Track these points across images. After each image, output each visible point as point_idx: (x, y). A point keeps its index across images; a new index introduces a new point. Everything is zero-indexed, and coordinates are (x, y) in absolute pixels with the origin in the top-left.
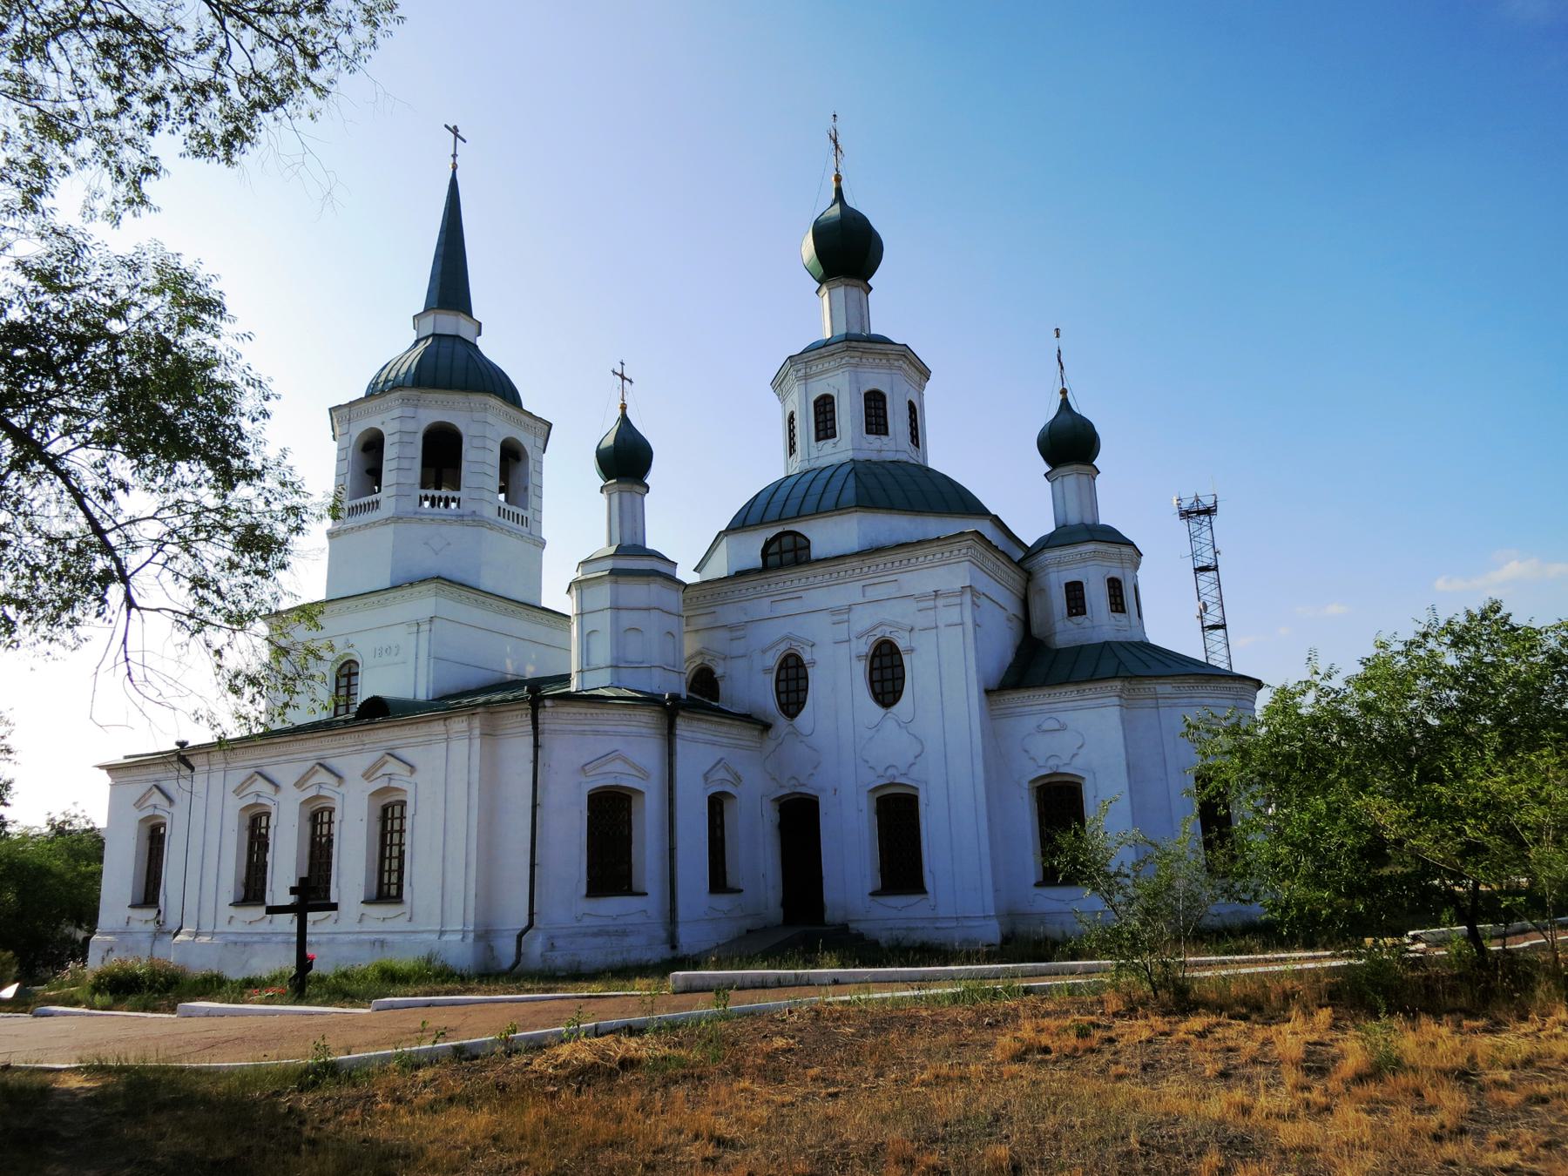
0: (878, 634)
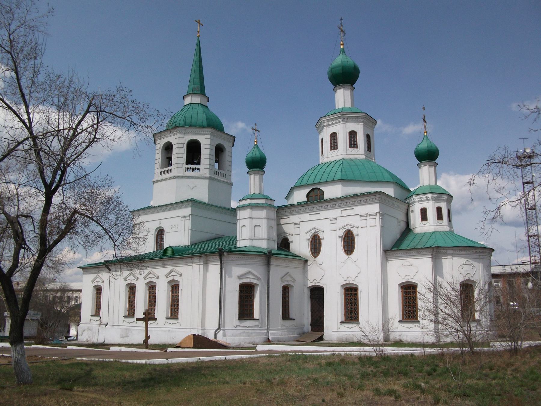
0: (346, 228)
